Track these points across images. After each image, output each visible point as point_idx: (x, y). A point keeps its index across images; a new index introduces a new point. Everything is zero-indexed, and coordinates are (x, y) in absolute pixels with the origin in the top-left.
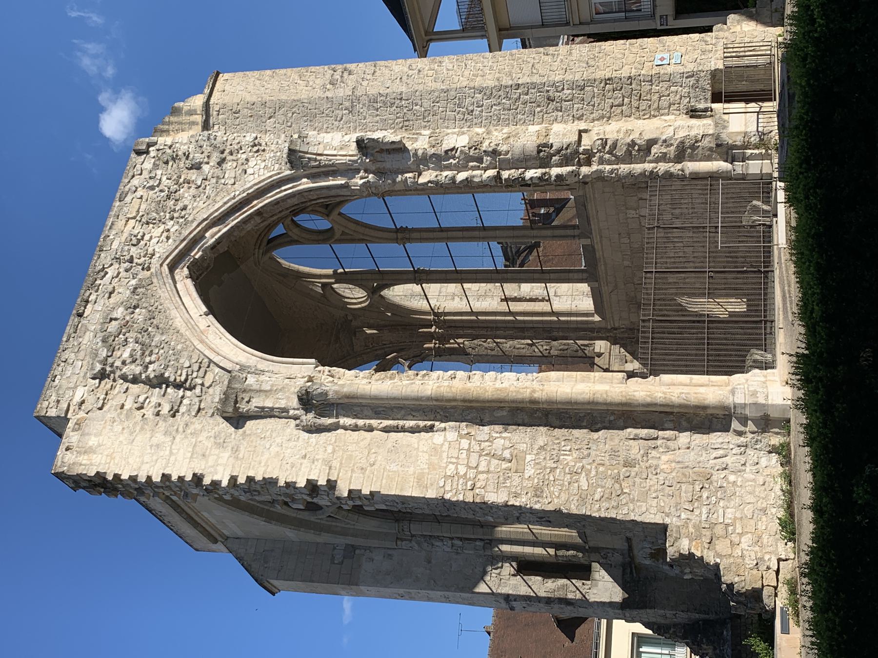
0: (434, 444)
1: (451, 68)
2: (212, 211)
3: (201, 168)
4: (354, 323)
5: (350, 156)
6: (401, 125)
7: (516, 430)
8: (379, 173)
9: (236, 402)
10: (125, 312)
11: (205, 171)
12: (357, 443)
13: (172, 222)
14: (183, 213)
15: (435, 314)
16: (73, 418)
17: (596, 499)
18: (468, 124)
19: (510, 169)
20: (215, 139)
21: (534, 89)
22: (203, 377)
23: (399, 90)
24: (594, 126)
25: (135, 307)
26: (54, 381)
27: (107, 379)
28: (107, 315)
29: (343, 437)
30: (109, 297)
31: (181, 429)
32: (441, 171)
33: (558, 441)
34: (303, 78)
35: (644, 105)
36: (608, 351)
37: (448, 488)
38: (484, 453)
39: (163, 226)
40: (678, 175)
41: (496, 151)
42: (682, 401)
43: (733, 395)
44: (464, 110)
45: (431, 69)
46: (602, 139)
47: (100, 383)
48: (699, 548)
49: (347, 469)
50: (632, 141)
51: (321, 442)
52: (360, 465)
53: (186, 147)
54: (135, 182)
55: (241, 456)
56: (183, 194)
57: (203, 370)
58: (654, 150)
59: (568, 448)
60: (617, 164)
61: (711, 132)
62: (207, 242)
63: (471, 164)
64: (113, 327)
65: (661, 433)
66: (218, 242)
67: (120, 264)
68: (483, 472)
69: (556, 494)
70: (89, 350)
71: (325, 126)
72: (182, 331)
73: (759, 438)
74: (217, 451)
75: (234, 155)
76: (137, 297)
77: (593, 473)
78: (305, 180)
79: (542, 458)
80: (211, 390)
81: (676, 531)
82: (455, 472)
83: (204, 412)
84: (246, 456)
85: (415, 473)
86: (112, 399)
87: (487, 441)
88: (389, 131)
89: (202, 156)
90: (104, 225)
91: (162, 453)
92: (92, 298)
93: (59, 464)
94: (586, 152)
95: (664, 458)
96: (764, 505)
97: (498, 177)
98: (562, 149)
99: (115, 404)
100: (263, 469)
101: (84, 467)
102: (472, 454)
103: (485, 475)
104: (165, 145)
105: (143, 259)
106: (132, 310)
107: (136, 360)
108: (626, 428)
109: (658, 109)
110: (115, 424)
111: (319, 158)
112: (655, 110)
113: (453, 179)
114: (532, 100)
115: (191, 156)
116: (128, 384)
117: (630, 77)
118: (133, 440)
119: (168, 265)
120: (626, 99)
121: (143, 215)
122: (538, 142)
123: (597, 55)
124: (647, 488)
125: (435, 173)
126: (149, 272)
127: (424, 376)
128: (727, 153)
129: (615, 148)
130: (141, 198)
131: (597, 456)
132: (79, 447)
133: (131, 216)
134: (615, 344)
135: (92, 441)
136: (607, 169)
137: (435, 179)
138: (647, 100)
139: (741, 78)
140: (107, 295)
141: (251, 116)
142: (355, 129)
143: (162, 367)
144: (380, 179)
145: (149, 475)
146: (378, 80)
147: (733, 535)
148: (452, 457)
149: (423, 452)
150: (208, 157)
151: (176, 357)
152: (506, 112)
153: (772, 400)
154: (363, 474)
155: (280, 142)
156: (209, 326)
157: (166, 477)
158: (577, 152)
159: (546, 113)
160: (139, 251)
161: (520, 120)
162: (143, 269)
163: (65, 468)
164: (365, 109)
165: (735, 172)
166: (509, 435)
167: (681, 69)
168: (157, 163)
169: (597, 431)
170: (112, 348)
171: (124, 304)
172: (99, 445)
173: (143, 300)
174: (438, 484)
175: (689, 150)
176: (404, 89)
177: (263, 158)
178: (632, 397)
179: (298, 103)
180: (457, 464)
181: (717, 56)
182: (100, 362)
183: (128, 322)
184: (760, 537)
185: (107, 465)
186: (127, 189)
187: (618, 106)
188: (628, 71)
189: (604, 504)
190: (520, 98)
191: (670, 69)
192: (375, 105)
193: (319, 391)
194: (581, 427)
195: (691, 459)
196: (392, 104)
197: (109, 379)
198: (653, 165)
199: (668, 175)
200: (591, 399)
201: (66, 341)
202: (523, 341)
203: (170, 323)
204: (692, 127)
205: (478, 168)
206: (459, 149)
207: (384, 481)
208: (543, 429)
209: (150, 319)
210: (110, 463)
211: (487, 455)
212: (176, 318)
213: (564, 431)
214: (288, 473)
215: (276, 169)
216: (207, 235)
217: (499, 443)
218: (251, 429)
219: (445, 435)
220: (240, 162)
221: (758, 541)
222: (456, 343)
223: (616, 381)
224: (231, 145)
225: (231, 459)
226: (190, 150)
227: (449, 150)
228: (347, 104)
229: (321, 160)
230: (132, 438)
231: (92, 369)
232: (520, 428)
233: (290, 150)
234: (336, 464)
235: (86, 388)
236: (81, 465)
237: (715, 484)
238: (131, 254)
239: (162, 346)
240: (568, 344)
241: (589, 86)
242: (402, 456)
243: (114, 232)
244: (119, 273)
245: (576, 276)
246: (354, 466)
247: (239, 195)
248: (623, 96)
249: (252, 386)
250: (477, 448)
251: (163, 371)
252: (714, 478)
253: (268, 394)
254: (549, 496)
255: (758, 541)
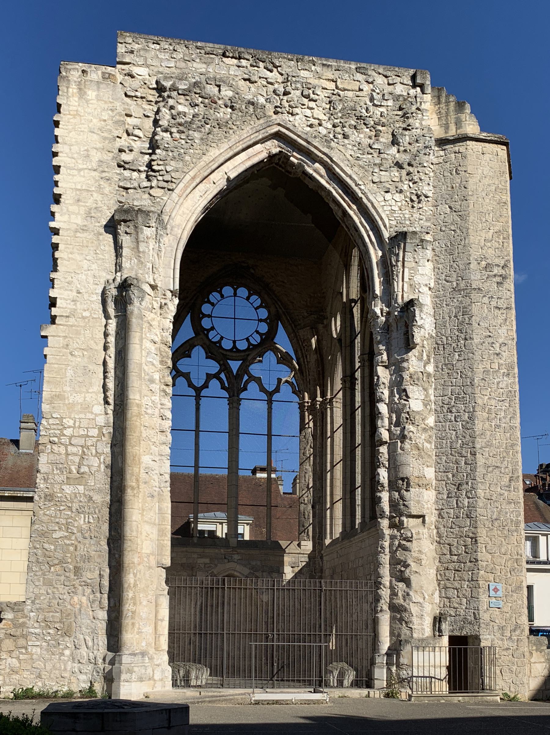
0: (93, 406)
1: (501, 385)
2: (342, 164)
3: (394, 145)
4: (320, 326)
5: (403, 295)
6: (440, 342)
7: (107, 475)
8: (387, 327)
9: (125, 221)
10: (227, 98)
11: (389, 150)
12: (92, 338)
13: (330, 126)
14: (340, 136)
15: (331, 399)
16: (117, 71)
17: (45, 545)
18: (439, 409)
19: (389, 453)
20: (425, 154)
21: (470, 470)
22: (158, 187)
23: (475, 336)
24: (429, 529)
25: (232, 107)
26: (154, 43)
27: (158, 95)
28: (224, 82)
29: (98, 324)
30: (245, 80)
31: (104, 175)
32: (389, 388)
33: (97, 512)
34: (495, 235)
35: (450, 574)
36: (302, 552)
37: (51, 421)
38: (85, 449)
39: (326, 118)
40: (377, 607)
41: (405, 438)
42: (125, 613)
43: (130, 654)
44: (453, 403)
45: (500, 365)
46: (412, 537)
47: (153, 89)
48: (5, 627)
49: (67, 331)
50: (409, 565)
51: (93, 306)
52: (71, 343)
53: (417, 125)
54: (380, 80)
55: (78, 234)
56: (362, 133)
57: (165, 185)
58: (401, 585)
59: (92, 521)
60: (390, 552)
61: (415, 635)
62: (309, 166)
63: (394, 416)
64: (212, 90)
65: (106, 596)
66: (311, 177)
67: (283, 83)
68: (67, 450)
69: (48, 512)
70: (186, 71)
71: (440, 266)
72: (205, 158)
73: (100, 674)
74: (82, 211)
75: (407, 177)
76: (244, 107)
77: (68, 542)
78: (380, 253)
79: (81, 499)
80: (147, 196)
81: (19, 609)
82: (66, 426)
83: (124, 194)
84: (78, 239)
85: (64, 392)
86: (137, 104)
87: (96, 451)
88: (435, 331)
89: (406, 144)
90: (328, 57)
91: (80, 161)
92: (244, 62)
93: (69, 67)
94: (401, 523)
95: (84, 599)
96: (43, 677)
97: (382, 443)
98: (404, 501)
99: (132, 108)
100: (66, 257)
101: (66, 91)
102: (84, 439)
103: (64, 452)
104: (421, 103)
105: (286, 105)
106: (229, 104)
107: (174, 119)
108: (110, 568)
109: (446, 588)
110: (110, 112)
111: (400, 264)
112: (445, 584)
113: (381, 400)
114: (459, 469)
115: (407, 133)
116: (154, 116)
117: (477, 560)
118: (94, 132)
119: (279, 131)
120: (456, 557)
121: (339, 96)
122: (412, 478)
123: (507, 528)
124: (56, 586)
125: (387, 382)
126: (272, 114)
127: (164, 391)
128: (395, 650)
129: (403, 550)
130: (360, 90)
131: (85, 544)
132: (85, 82)
133: (338, 83)
134: (309, 557)
135: (91, 94)
136: (385, 543)
137: (380, 382)
138: (454, 577)
139: (476, 663)
140: (246, 77)
141: (453, 188)
142: (437, 297)
143: (166, 146)
144: (381, 329)
145: (59, 154)
146: (489, 313)
147: (18, 652)
148: (80, 422)
149: (85, 397)
150: (405, 151)
151: (177, 157)
152: (449, 445)
153: (124, 685)
154: (63, 347)
155: (422, 222)
156: (214, 183)
157: (57, 169)
158: (401, 515)
159: (446, 484)
160: (296, 99)
161: (441, 459)
162: (276, 107)
163: (64, 74)
164: (457, 304)
165: (377, 657)
166: (102, 470)
167: (483, 606)
168: (401, 99)
169: (109, 544)
170: (187, 93)
171: (237, 96)
172: (87, 101)
173: (240, 114)
174: (55, 412)
175: (399, 616)
176: (477, 340)
177: (403, 207)
178: (128, 572)
179: (465, 234)
180: (74, 428)
181: (496, 641)
182: (173, 85)
183: (215, 103)
184: (17, 673)
185: (67, 113)
186: (370, 72)
187: (450, 551)
188: (483, 559)
189: (40, 551)
190: (462, 457)
191: (484, 598)
192: (460, 314)
193: (132, 296)
194: (110, 530)
195: (83, 621)
196: (460, 331)
197: (158, 97)
198: (388, 584)
199: (377, 599)
200: (126, 538)
201: (196, 47)
202: (311, 480)
203: (213, 145)
204: (421, 618)
205: (390, 423)
206: (407, 403)
207: (56, 366)
208: (108, 498)
209: (218, 125)
210: (69, 114)
211: (83, 452)
212: (219, 149)
213: (107, 516)
214: (63, 280)
215: (391, 222)
216: (317, 165)
217: (95, 462)
218: (104, 240)
219: (101, 414)
220: (400, 185)
221: (14, 671)
222: (310, 421)
223: (160, 558)
224: (418, 172)
225: (75, 226)
226: (414, 130)
227: (406, 392)
228: (462, 285)
229: (398, 266)
230: (96, 131)
231: (166, 78)
232: (109, 479)
233: (406, 233)
234: (72, 321)
235: (148, 77)
236: (68, 88)
237: (61, 639)
238: (292, 92)
239: (188, 141)
240: (309, 518)
241: (470, 522)
242: (80, 379)
243: (319, 69)
244: (272, 84)
245: (348, 521)
246: (71, 338)
247: (360, 189)
248: (459, 555)
249: (141, 233)
250: (89, 443)
251: (161, 147)
252: (67, 639)
253: (135, 250)
254: (46, 506)
255: (14, 671)
